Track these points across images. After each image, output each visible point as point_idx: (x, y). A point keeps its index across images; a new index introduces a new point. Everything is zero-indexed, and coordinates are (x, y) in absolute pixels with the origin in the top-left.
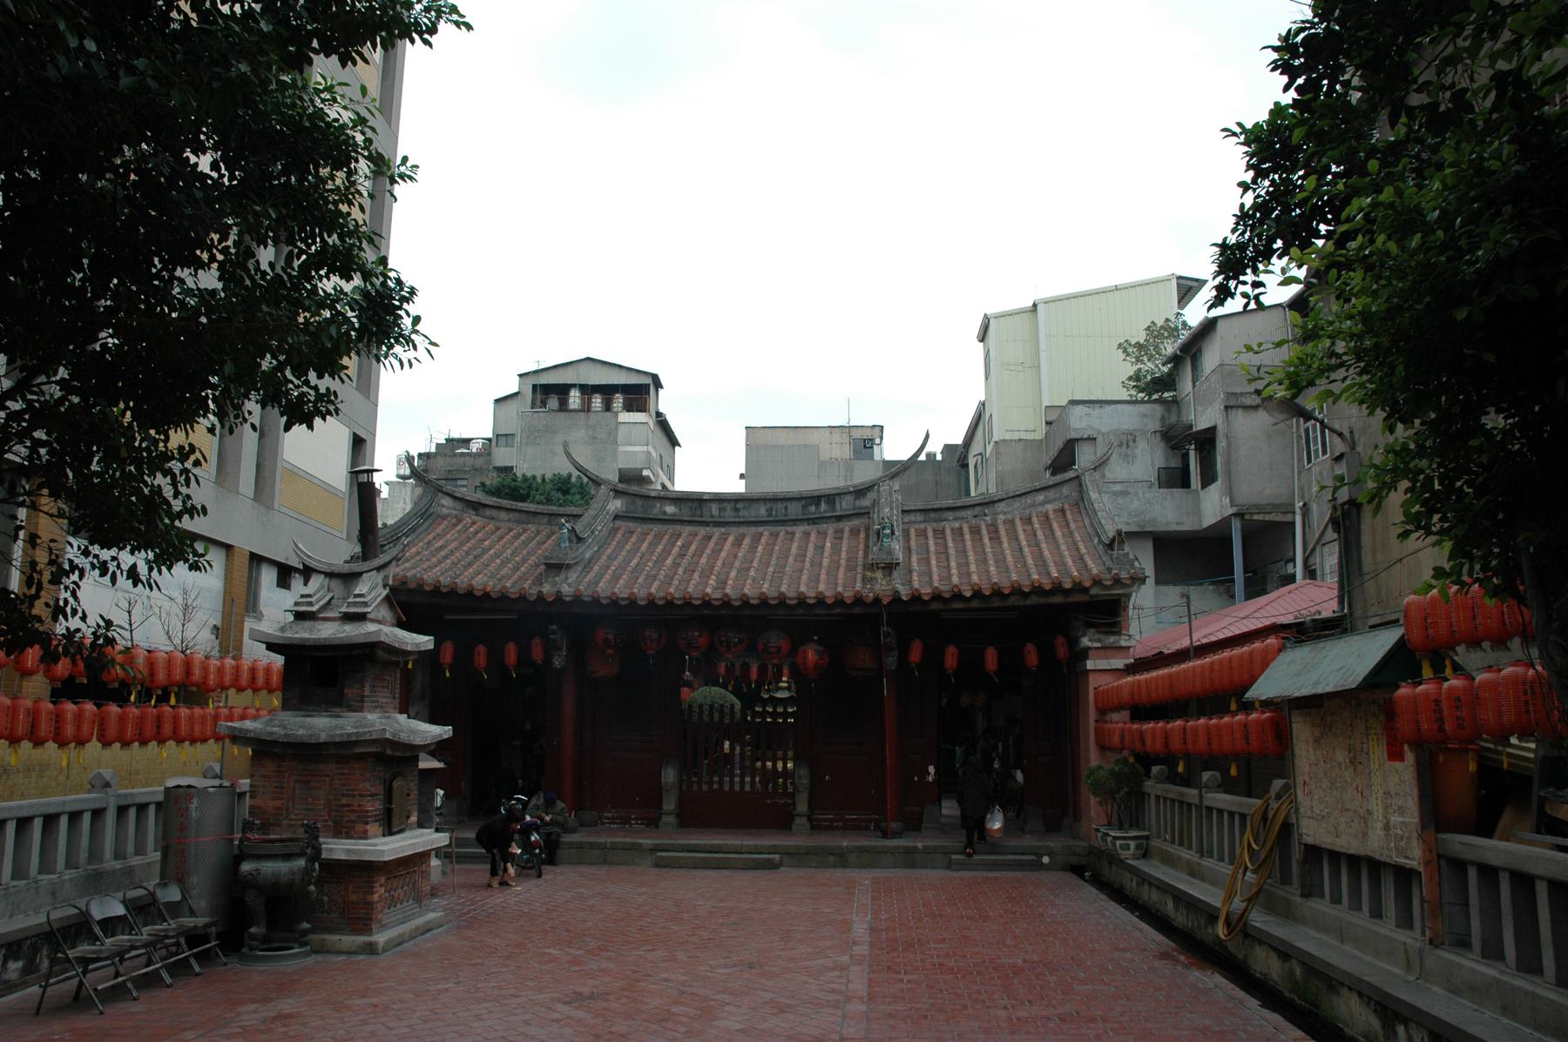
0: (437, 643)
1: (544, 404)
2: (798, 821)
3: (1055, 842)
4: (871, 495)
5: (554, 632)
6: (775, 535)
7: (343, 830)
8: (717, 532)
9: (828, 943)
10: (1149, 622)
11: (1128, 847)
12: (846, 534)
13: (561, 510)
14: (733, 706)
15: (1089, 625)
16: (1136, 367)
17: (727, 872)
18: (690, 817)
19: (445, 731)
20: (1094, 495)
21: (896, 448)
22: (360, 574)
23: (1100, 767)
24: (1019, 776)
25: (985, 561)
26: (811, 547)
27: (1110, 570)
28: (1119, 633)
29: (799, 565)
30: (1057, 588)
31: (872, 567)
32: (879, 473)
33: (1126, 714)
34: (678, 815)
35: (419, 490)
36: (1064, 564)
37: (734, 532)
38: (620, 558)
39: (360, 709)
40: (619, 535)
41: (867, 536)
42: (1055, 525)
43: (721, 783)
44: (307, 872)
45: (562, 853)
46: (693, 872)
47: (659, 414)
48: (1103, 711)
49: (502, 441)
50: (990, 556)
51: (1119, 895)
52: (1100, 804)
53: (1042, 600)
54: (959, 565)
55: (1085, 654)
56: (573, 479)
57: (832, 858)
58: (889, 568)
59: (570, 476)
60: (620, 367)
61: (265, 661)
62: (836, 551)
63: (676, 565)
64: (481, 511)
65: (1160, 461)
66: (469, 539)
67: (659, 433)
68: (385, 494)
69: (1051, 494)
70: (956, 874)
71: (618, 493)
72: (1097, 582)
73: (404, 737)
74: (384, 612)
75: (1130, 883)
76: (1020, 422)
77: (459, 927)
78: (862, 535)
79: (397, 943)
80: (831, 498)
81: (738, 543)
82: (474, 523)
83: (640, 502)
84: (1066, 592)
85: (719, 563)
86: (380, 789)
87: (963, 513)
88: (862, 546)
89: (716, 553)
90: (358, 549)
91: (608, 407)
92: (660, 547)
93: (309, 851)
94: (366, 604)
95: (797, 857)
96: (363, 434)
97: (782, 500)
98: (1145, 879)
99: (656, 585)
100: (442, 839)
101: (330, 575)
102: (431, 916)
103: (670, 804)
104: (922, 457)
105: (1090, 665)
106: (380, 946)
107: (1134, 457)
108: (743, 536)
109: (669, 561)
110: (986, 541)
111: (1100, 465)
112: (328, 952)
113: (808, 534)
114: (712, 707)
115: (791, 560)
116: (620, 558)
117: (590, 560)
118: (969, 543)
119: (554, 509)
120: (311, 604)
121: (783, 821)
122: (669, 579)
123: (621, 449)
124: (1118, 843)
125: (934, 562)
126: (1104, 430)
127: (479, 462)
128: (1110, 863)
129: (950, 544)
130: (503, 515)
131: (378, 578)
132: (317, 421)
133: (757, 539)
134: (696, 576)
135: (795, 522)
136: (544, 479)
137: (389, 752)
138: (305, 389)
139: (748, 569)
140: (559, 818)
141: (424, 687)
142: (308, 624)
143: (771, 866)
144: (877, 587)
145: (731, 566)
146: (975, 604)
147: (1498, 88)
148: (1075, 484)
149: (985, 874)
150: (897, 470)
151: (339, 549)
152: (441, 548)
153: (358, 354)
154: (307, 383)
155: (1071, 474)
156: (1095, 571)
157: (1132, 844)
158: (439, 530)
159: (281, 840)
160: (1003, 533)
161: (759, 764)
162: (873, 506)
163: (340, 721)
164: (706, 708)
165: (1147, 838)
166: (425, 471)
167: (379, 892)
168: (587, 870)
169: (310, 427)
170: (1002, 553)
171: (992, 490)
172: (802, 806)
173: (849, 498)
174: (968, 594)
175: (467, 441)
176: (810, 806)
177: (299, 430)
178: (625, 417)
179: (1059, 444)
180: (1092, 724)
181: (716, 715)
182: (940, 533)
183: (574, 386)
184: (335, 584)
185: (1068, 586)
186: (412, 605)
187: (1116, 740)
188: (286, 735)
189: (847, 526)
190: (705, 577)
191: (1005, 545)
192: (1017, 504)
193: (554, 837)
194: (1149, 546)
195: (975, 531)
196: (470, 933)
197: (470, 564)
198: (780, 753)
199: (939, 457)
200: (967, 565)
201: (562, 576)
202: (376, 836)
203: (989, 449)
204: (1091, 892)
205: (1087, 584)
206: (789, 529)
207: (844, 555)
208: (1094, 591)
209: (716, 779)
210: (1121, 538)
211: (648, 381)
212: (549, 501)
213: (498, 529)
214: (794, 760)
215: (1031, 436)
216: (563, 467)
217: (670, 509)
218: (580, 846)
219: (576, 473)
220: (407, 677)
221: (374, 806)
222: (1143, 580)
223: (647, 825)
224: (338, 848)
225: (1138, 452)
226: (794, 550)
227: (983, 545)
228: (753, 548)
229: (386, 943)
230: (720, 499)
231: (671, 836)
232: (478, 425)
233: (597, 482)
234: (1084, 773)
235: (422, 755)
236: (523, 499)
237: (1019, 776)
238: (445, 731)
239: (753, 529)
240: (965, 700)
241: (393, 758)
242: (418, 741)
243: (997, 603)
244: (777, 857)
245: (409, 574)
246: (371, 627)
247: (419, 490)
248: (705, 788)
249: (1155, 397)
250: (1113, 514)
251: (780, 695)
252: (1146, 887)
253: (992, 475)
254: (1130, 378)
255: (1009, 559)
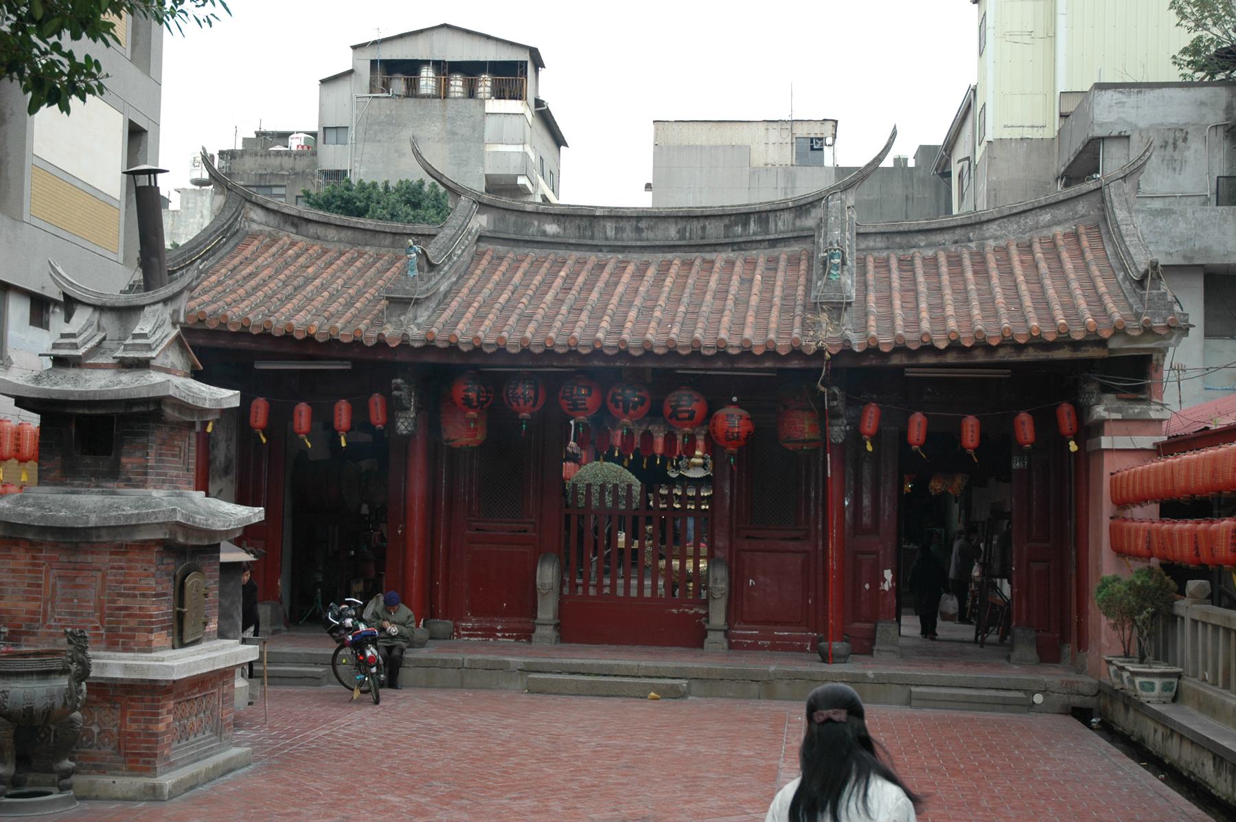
0: (243, 399)
1: (386, 86)
2: (711, 636)
3: (1053, 676)
4: (817, 213)
5: (398, 388)
6: (689, 264)
7: (118, 640)
8: (613, 259)
9: (746, 796)
10: (1192, 388)
11: (1151, 687)
12: (782, 264)
13: (409, 228)
14: (629, 486)
15: (1106, 389)
16: (1194, 35)
17: (618, 701)
18: (579, 625)
19: (255, 514)
20: (1121, 214)
21: (851, 152)
22: (141, 308)
23: (1116, 579)
24: (1006, 589)
25: (967, 301)
26: (735, 281)
27: (1138, 316)
28: (1147, 401)
29: (718, 303)
30: (1064, 341)
31: (815, 308)
32: (828, 182)
33: (1153, 509)
34: (556, 626)
35: (220, 200)
36: (1074, 307)
37: (636, 258)
38: (486, 291)
39: (143, 484)
40: (484, 262)
41: (810, 269)
42: (1065, 255)
43: (613, 586)
44: (70, 694)
45: (405, 674)
46: (576, 700)
47: (539, 103)
48: (1122, 503)
49: (331, 135)
50: (973, 295)
51: (1137, 750)
52: (1114, 627)
53: (1042, 355)
54: (931, 307)
55: (1099, 427)
56: (426, 189)
57: (755, 686)
58: (838, 308)
59: (421, 183)
60: (488, 37)
61: (14, 422)
62: (768, 285)
63: (558, 301)
64: (303, 228)
65: (1220, 168)
66: (287, 265)
67: (539, 128)
68: (175, 205)
69: (1061, 212)
70: (917, 713)
71: (483, 207)
72: (1119, 331)
73: (200, 520)
74: (174, 358)
75: (1154, 737)
76: (1021, 113)
77: (270, 767)
78: (803, 266)
79: (190, 785)
80: (763, 215)
81: (640, 274)
82: (293, 244)
83: (512, 218)
84: (1076, 345)
85: (615, 300)
86: (169, 587)
87: (938, 238)
88: (802, 280)
89: (611, 285)
90: (139, 276)
91: (471, 93)
92: (539, 278)
93: (74, 667)
94: (149, 347)
95: (709, 683)
96: (141, 122)
97: (697, 217)
98: (1173, 731)
99: (532, 327)
100: (250, 652)
101: (100, 308)
102: (234, 752)
103: (547, 611)
104: (888, 162)
105: (1105, 442)
106: (166, 791)
107: (1183, 162)
108: (647, 264)
109: (549, 297)
110: (969, 274)
111: (1132, 173)
112: (97, 798)
113: (731, 264)
114: (603, 487)
115: (708, 297)
116: (486, 291)
117: (446, 295)
118: (945, 278)
119: (398, 226)
120: (75, 346)
121: (692, 635)
122: (549, 320)
123: (490, 148)
124: (1138, 680)
125: (897, 303)
126: (1142, 124)
127: (301, 165)
128: (1127, 707)
129: (921, 278)
130: (332, 233)
131: (165, 312)
132: (74, 101)
133: (664, 269)
134: (584, 316)
135: (715, 247)
136: (386, 188)
137: (181, 540)
138: (56, 56)
139: (652, 309)
140: (405, 631)
141: (241, 458)
142: (71, 372)
143: (675, 694)
144: (821, 335)
145: (630, 304)
146: (951, 358)
147: (743, 353)
148: (1095, 198)
149: (955, 714)
150: (851, 179)
151: (114, 276)
152: (251, 275)
153: (131, 11)
154: (57, 47)
155: (1091, 185)
156: (1117, 317)
157: (1158, 682)
158: (248, 252)
159: (37, 654)
160: (992, 264)
161: (662, 563)
162: (819, 227)
163: (116, 499)
164: (595, 489)
165: (1179, 676)
166: (230, 175)
167: (166, 721)
168: (438, 695)
169: (65, 108)
170: (991, 292)
171: (982, 205)
172: (718, 617)
173: (787, 216)
174: (942, 345)
175: (284, 136)
176: (728, 619)
177: (49, 113)
178: (494, 106)
179: (1077, 145)
180: (1106, 522)
181: (609, 499)
182: (907, 265)
183: (426, 62)
184: (108, 321)
185: (1078, 335)
186: (212, 350)
187: (1141, 544)
188: (43, 517)
189: (783, 252)
190: (596, 316)
191: (995, 281)
192: (1013, 226)
193: (396, 652)
194: (1198, 285)
195: (955, 262)
196: (284, 774)
197: (289, 298)
198: (690, 550)
199: (911, 163)
200: (942, 307)
201: (410, 315)
202: (162, 649)
203: (980, 151)
204: (1100, 744)
205: (1105, 334)
206: (708, 256)
207: (778, 291)
208: (1113, 345)
209: (607, 581)
210: (1156, 272)
211: (524, 56)
212: (393, 216)
213: (325, 252)
214: (710, 557)
215: (1037, 134)
216: (414, 173)
217: (551, 228)
218: (429, 664)
219: (429, 180)
220: (206, 443)
221: (162, 609)
222: (1185, 330)
223: (518, 638)
224: (112, 664)
225: (1189, 154)
226: (713, 284)
227: (965, 281)
228: (659, 281)
229: (175, 786)
230: (617, 216)
231: (545, 649)
232: (299, 115)
233: (455, 191)
234: (1094, 585)
235: (224, 544)
236: (361, 213)
237: (1006, 589)
238: (255, 514)
239: (660, 256)
240: (936, 486)
241: (187, 549)
242: (219, 526)
243: (980, 357)
244: (684, 683)
245: (208, 310)
246: (156, 378)
247: (220, 200)
248: (592, 592)
249: (1220, 76)
250: (1147, 237)
251: (692, 474)
252: (1176, 740)
253: (983, 188)
254: (1185, 51)
255: (1000, 298)
